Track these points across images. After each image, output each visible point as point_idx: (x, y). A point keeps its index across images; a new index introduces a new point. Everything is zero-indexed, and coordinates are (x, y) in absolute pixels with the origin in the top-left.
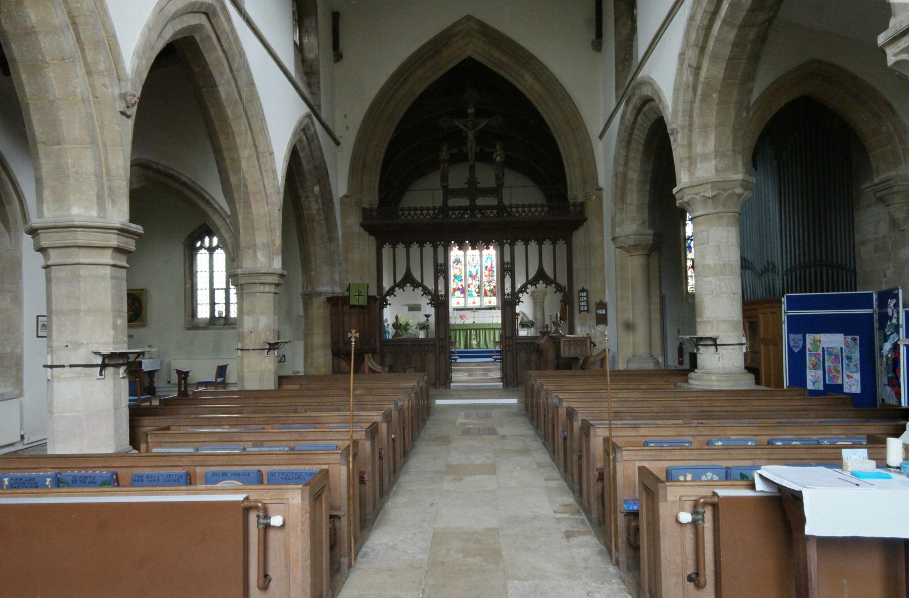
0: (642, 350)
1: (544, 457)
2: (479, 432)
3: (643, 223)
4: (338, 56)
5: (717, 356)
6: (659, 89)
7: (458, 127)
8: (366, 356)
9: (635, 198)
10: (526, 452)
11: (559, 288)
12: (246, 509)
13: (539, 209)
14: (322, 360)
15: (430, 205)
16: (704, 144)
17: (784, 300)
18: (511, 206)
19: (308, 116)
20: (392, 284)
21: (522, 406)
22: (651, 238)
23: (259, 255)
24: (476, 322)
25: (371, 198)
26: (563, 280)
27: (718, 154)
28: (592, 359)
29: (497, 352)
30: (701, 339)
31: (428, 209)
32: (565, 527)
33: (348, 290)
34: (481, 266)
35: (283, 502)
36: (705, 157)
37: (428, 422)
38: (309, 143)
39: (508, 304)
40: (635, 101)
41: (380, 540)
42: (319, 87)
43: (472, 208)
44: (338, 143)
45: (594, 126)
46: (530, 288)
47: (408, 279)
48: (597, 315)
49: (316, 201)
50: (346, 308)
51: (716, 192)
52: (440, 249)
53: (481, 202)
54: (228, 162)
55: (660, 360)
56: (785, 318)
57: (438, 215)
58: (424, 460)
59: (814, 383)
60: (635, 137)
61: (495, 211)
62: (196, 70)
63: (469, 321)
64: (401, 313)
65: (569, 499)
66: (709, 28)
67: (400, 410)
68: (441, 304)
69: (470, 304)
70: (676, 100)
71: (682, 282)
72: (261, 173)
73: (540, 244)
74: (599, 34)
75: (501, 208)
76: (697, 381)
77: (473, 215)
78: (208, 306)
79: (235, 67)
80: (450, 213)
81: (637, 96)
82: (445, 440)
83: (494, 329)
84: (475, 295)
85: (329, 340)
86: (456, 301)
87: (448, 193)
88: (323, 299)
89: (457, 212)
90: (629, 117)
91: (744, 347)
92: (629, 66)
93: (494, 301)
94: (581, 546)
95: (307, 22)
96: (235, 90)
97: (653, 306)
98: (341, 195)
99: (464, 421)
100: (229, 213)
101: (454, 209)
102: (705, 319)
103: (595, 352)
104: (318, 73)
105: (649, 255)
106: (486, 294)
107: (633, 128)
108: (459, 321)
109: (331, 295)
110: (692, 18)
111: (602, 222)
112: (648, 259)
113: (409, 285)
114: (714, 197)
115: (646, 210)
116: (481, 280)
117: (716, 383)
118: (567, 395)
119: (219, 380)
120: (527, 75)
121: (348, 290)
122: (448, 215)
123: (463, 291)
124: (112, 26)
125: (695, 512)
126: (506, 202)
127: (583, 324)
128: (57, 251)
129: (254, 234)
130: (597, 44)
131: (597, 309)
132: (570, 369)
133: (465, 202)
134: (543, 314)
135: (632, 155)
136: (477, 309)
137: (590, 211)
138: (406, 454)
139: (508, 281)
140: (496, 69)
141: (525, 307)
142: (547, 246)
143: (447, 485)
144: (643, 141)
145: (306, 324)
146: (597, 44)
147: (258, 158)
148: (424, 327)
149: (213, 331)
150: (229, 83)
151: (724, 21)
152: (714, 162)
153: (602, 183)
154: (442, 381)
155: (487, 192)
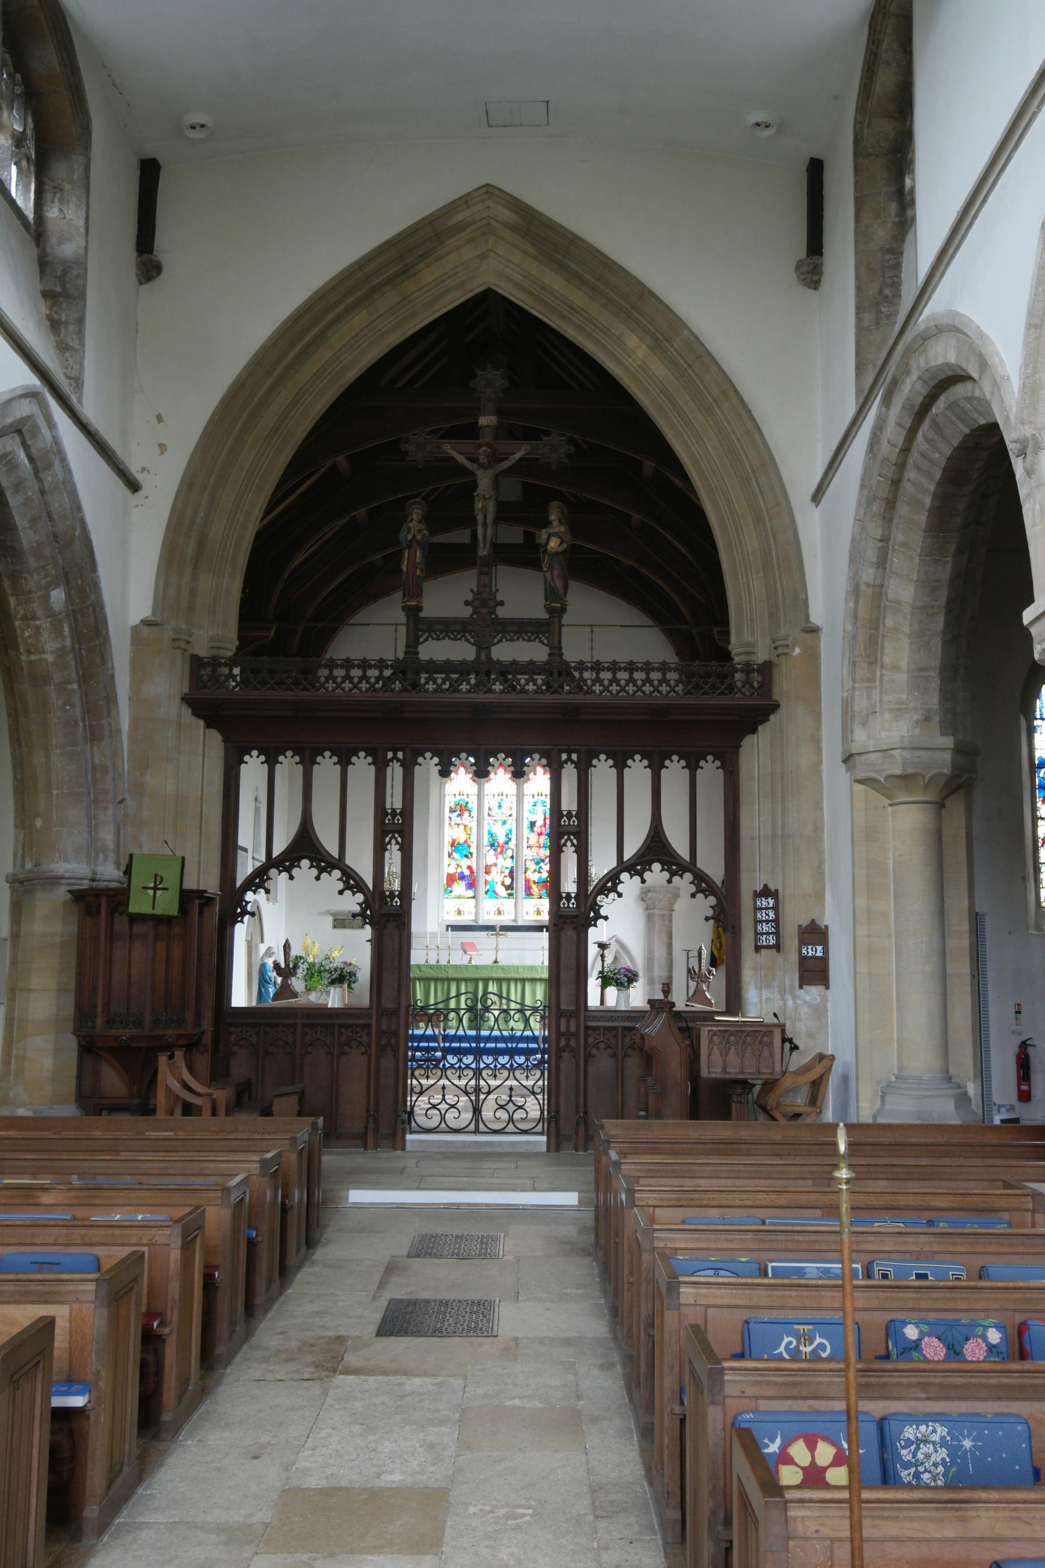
0: (922, 1059)
3: (927, 719)
4: (149, 269)
6: (982, 335)
7: (452, 459)
9: (907, 654)
11: (703, 884)
13: (656, 676)
14: (48, 1062)
18: (581, 666)
21: (588, 1217)
22: (947, 756)
24: (503, 961)
25: (218, 630)
28: (787, 1082)
33: (128, 872)
38: (36, 472)
39: (571, 924)
40: (911, 388)
42: (80, 332)
43: (485, 669)
44: (134, 486)
45: (799, 465)
46: (629, 884)
47: (305, 848)
49: (57, 630)
50: (121, 924)
52: (395, 773)
53: (504, 651)
55: (972, 1089)
60: (907, 487)
61: (539, 679)
64: (290, 934)
68: (388, 916)
69: (488, 917)
71: (1024, 878)
73: (656, 769)
74: (815, 244)
75: (557, 670)
77: (482, 685)
81: (915, 375)
83: (533, 980)
84: (502, 891)
85: (70, 1010)
87: (420, 627)
88: (61, 894)
89: (439, 677)
90: (894, 434)
92: (891, 317)
95: (60, 170)
97: (951, 943)
101: (433, 667)
103: (797, 1061)
104: (82, 296)
105: (941, 805)
106: (529, 892)
107: (901, 467)
109: (86, 884)
111: (817, 716)
113: (305, 863)
115: (936, 685)
120: (632, 341)
122: (415, 685)
126: (571, 655)
127: (765, 983)
132: (726, 1116)
133: (461, 651)
134: (670, 946)
135: (898, 536)
137: (786, 685)
141: (620, 925)
144: (928, 501)
145: (14, 963)
146: (811, 267)
153: (817, 615)
154: (383, 1125)
155: (523, 629)
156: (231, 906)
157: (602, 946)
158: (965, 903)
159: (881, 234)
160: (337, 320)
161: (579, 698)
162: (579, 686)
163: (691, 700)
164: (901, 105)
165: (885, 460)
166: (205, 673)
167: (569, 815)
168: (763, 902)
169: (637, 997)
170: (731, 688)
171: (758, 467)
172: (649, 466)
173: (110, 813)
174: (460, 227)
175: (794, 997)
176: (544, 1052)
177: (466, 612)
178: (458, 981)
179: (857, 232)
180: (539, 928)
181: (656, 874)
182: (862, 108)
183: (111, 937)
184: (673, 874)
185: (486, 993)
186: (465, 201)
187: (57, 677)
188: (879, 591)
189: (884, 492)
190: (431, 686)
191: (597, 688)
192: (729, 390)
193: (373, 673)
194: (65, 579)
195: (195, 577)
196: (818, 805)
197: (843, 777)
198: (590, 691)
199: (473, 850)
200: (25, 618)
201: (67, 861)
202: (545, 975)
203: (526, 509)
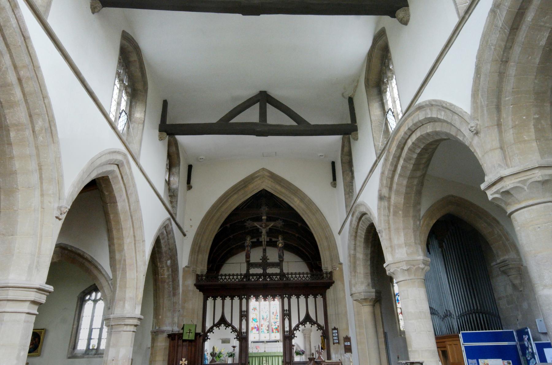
3: (368, 285)
4: (189, 187)
11: (320, 327)
15: (239, 273)
17: (460, 335)
18: (288, 274)
19: (169, 219)
22: (374, 294)
23: (127, 305)
24: (266, 351)
25: (202, 268)
31: (237, 275)
33: (183, 329)
34: (270, 312)
36: (400, 246)
38: (167, 235)
39: (288, 338)
40: (357, 214)
42: (177, 204)
43: (265, 275)
44: (185, 235)
45: (335, 227)
46: (301, 327)
47: (223, 321)
48: (345, 346)
49: (168, 270)
51: (409, 267)
52: (244, 301)
53: (270, 271)
54: (116, 246)
56: (463, 349)
61: (278, 277)
62: (107, 193)
66: (392, 178)
68: (243, 338)
69: (262, 339)
71: (396, 323)
72: (136, 252)
73: (307, 298)
74: (334, 179)
75: (282, 275)
77: (265, 279)
80: (251, 277)
83: (278, 356)
84: (266, 332)
86: (253, 336)
87: (250, 265)
88: (165, 335)
89: (255, 277)
90: (355, 223)
93: (278, 336)
95: (174, 170)
98: (184, 266)
100: (111, 277)
101: (253, 275)
102: (413, 349)
104: (177, 196)
105: (374, 306)
107: (357, 229)
109: (171, 333)
110: (383, 173)
111: (343, 284)
113: (223, 325)
114: (408, 270)
115: (370, 277)
116: (269, 322)
120: (296, 199)
121: (183, 329)
122: (249, 279)
126: (285, 271)
127: (336, 353)
129: (125, 292)
133: (260, 271)
134: (310, 345)
135: (358, 244)
137: (336, 277)
142: (311, 299)
144: (363, 237)
145: (152, 354)
148: (231, 355)
150: (124, 201)
152: (405, 249)
153: (342, 260)
155: (273, 265)
158: (382, 330)
159: (348, 179)
160: (231, 197)
161: (287, 282)
162: (287, 278)
163: (314, 281)
164: (350, 154)
165: (353, 228)
166: (200, 278)
167: (286, 310)
168: (335, 331)
170: (323, 278)
171: (326, 227)
172: (300, 224)
173: (177, 314)
174: (257, 177)
175: (344, 356)
178: (255, 357)
179: (343, 179)
181: (308, 325)
182: (342, 154)
183: (178, 346)
184: (312, 325)
186: (258, 172)
187: (167, 281)
189: (354, 234)
190: (253, 280)
191: (292, 279)
192: (318, 210)
193: (239, 277)
194: (171, 258)
195: (198, 256)
196: (345, 306)
198: (290, 280)
199: (258, 320)
200: (161, 268)
201: (167, 326)
203: (272, 232)
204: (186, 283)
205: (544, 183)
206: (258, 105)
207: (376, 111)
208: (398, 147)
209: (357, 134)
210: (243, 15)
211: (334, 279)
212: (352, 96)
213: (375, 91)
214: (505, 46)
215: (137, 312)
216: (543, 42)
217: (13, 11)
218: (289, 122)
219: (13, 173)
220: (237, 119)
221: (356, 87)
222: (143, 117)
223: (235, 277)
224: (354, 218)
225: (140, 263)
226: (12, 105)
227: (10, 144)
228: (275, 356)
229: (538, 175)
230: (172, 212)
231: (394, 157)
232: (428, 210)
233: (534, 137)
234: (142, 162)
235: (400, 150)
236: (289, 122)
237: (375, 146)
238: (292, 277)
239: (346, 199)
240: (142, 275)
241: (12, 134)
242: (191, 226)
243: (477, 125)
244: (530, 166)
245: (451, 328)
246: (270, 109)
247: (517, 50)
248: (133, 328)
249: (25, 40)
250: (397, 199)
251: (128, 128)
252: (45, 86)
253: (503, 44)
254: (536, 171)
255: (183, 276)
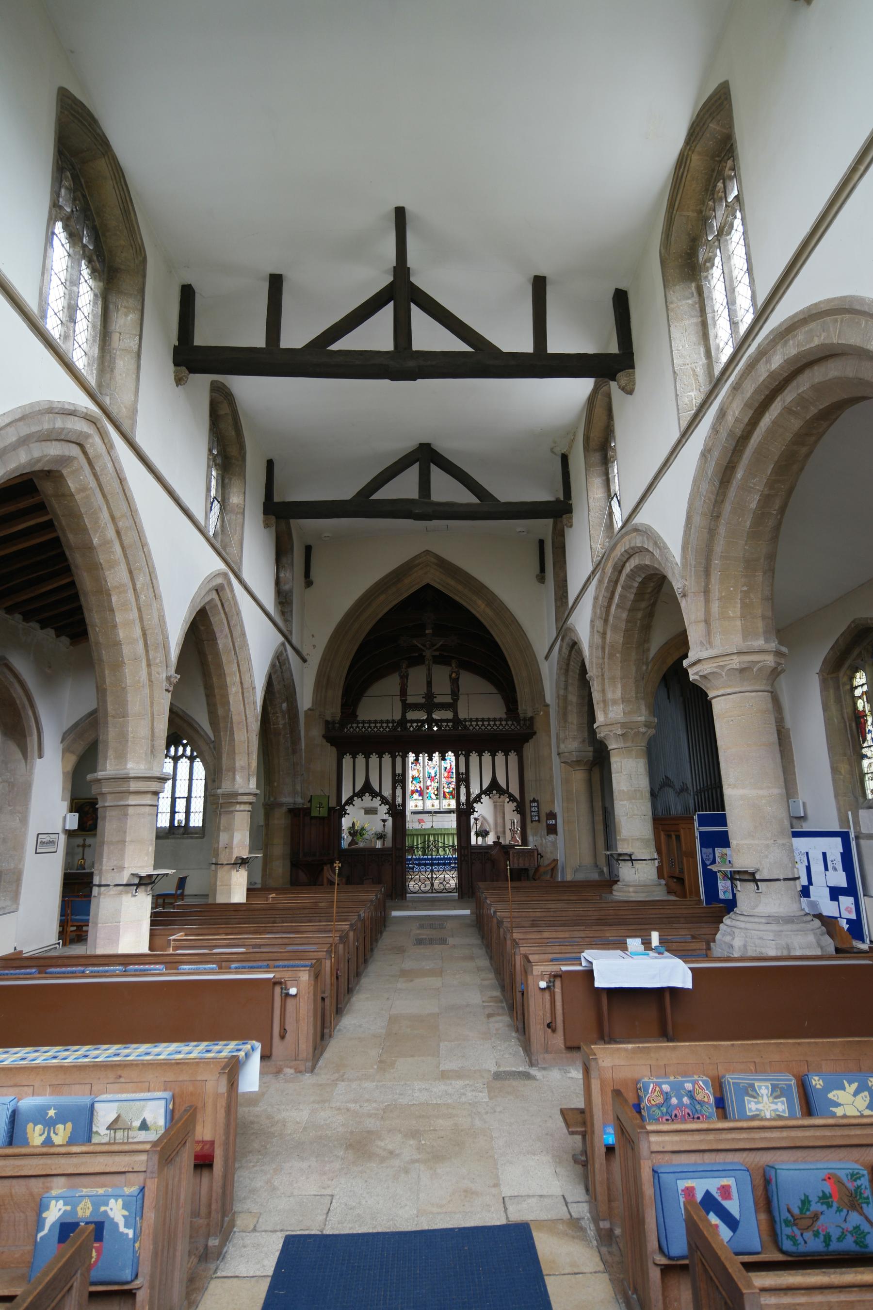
0: (588, 860)
1: (485, 963)
2: (431, 942)
3: (584, 741)
5: (633, 870)
8: (325, 868)
10: (471, 958)
11: (512, 798)
12: (276, 983)
14: (280, 870)
15: (390, 718)
16: (614, 692)
17: (696, 817)
19: (283, 644)
20: (351, 794)
21: (474, 918)
22: (591, 754)
23: (238, 777)
24: (435, 827)
25: (334, 711)
26: (516, 793)
27: (624, 700)
28: (542, 870)
29: (455, 859)
30: (620, 855)
31: (387, 722)
32: (487, 1011)
33: (310, 801)
35: (296, 981)
36: (615, 702)
37: (385, 934)
39: (464, 813)
41: (348, 1022)
42: (292, 615)
47: (367, 789)
48: (548, 825)
49: (284, 717)
52: (399, 760)
55: (605, 870)
56: (697, 834)
57: (397, 726)
58: (381, 967)
59: (724, 893)
60: (571, 667)
61: (450, 724)
62: (202, 628)
63: (427, 825)
64: (364, 821)
65: (497, 993)
67: (363, 921)
68: (398, 813)
70: (591, 654)
72: (244, 705)
73: (367, 758)
74: (542, 569)
75: (456, 721)
76: (619, 893)
78: (169, 815)
79: (232, 623)
82: (400, 950)
84: (434, 797)
86: (413, 804)
87: (406, 707)
89: (415, 725)
90: (565, 651)
91: (656, 862)
93: (453, 804)
94: (497, 1022)
96: (230, 641)
98: (305, 708)
99: (418, 932)
100: (213, 739)
101: (412, 721)
103: (547, 862)
105: (590, 771)
106: (445, 797)
107: (569, 659)
108: (417, 826)
109: (292, 807)
110: (596, 598)
112: (590, 773)
113: (367, 794)
117: (633, 894)
118: (501, 907)
119: (179, 892)
120: (480, 602)
121: (310, 801)
122: (406, 728)
123: (421, 794)
124: (167, 632)
125: (549, 982)
126: (462, 715)
127: (535, 834)
128: (113, 795)
129: (234, 759)
130: (541, 577)
131: (547, 819)
134: (504, 818)
135: (570, 681)
136: (436, 812)
137: (538, 725)
138: (358, 975)
139: (463, 790)
140: (451, 595)
142: (500, 757)
143: (401, 984)
145: (267, 835)
146: (541, 577)
147: (243, 693)
148: (381, 836)
149: (173, 841)
150: (226, 636)
151: (617, 605)
152: (621, 706)
154: (398, 892)
156: (341, 812)
157: (476, 819)
162: (465, 726)
166: (330, 726)
169: (490, 840)
171: (525, 647)
176: (455, 863)
177: (423, 701)
178: (417, 835)
180: (450, 812)
185: (429, 841)
188: (565, 698)
190: (411, 729)
191: (471, 728)
192: (514, 621)
193: (390, 725)
197: (558, 760)
202: (455, 832)
204: (311, 734)
205: (742, 671)
206: (416, 466)
207: (597, 493)
208: (614, 568)
209: (571, 518)
210: (392, 379)
211: (535, 729)
212: (567, 453)
213: (596, 457)
214: (716, 501)
215: (252, 785)
216: (753, 505)
217: (109, 453)
218: (466, 497)
219: (118, 644)
220: (384, 493)
221: (573, 440)
222: (242, 502)
223: (384, 725)
224: (565, 645)
225: (251, 719)
226: (113, 564)
227: (112, 610)
228: (448, 834)
229: (735, 662)
230: (286, 633)
231: (610, 581)
232: (661, 648)
233: (739, 614)
234: (245, 576)
235: (616, 573)
236: (466, 497)
237: (591, 548)
238: (471, 725)
239: (557, 607)
240: (254, 736)
241: (114, 599)
242: (314, 646)
243: (685, 586)
244: (729, 651)
245: (687, 809)
246: (437, 474)
247: (727, 507)
248: (248, 807)
249: (121, 482)
250: (615, 638)
251: (223, 521)
252: (143, 532)
253: (713, 497)
254: (735, 657)
255: (305, 723)
